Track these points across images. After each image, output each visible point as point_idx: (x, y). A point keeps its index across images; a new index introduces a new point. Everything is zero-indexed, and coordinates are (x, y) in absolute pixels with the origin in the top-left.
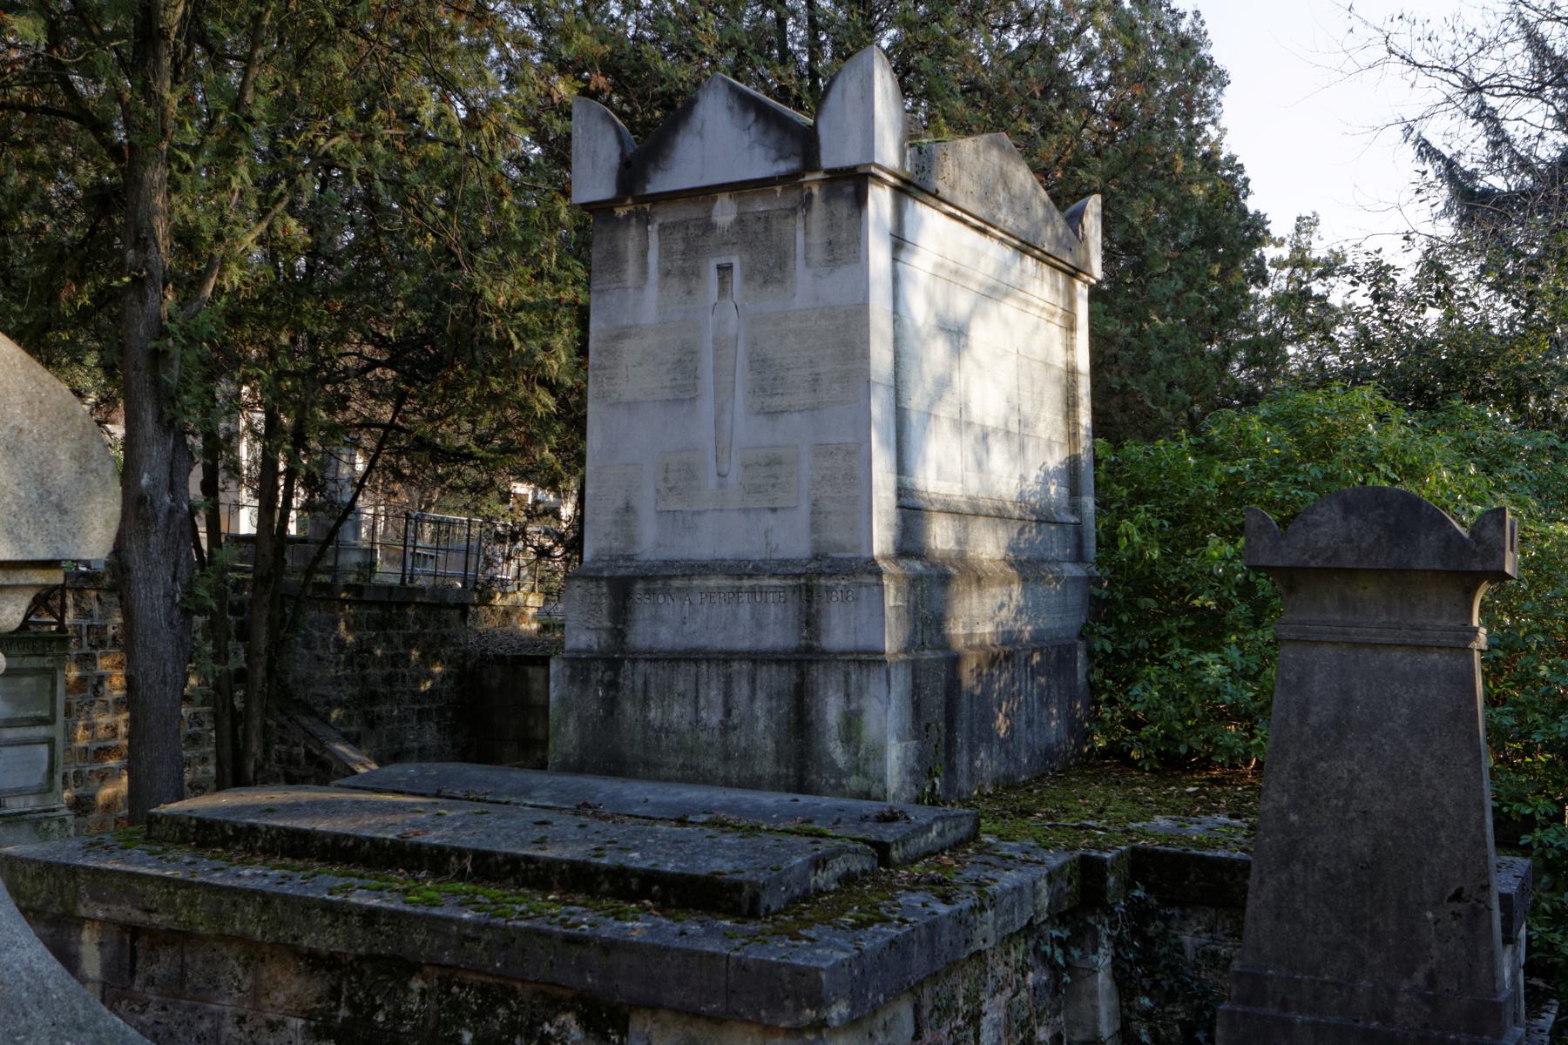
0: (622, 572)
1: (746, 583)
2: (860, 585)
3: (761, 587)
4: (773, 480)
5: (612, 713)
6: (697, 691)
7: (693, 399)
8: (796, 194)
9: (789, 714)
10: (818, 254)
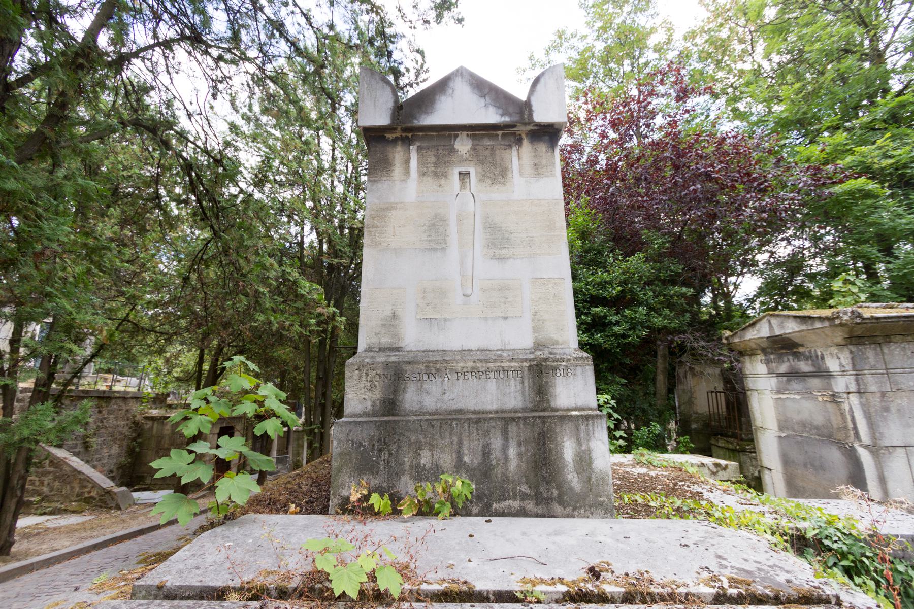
7: (444, 249)
10: (528, 170)
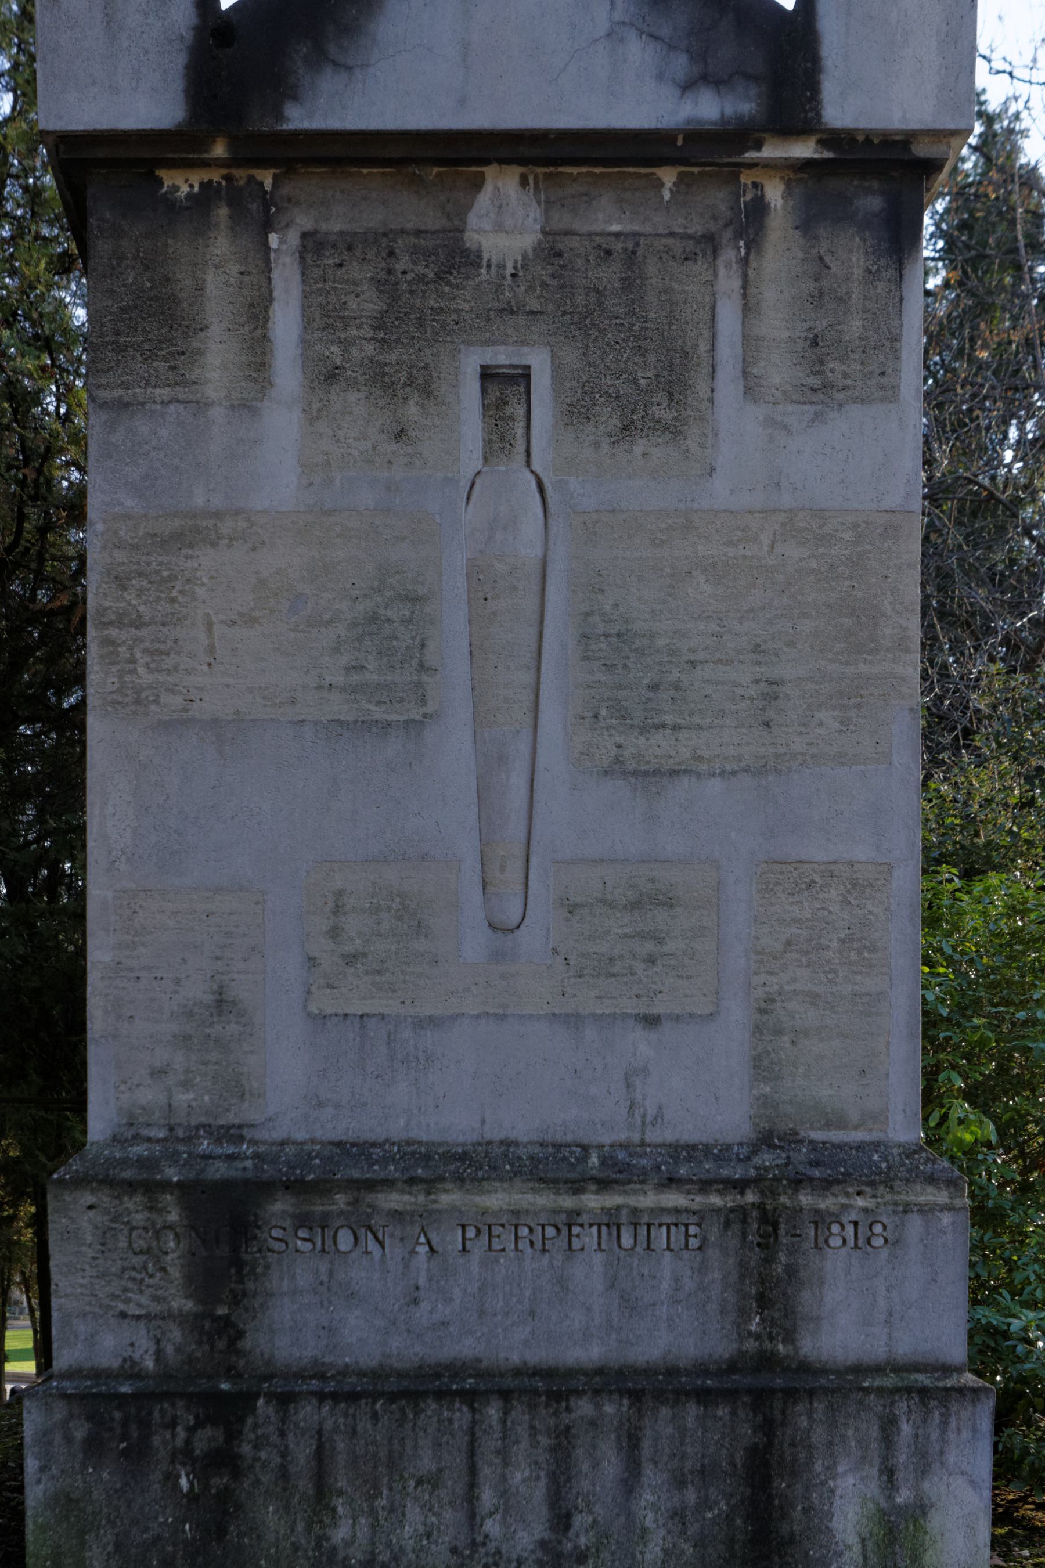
0: (218, 1171)
1: (593, 1201)
2: (907, 1209)
3: (635, 1211)
4: (649, 946)
5: (221, 1532)
6: (473, 1471)
8: (718, 198)
9: (729, 1518)
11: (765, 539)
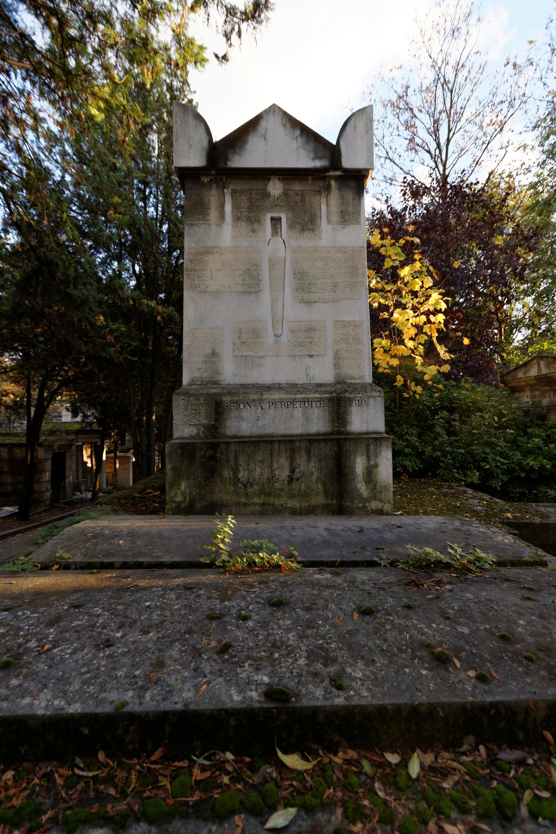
1: (299, 396)
2: (370, 397)
3: (308, 398)
4: (310, 340)
7: (257, 292)
8: (321, 183)
10: (335, 218)
11: (333, 253)
